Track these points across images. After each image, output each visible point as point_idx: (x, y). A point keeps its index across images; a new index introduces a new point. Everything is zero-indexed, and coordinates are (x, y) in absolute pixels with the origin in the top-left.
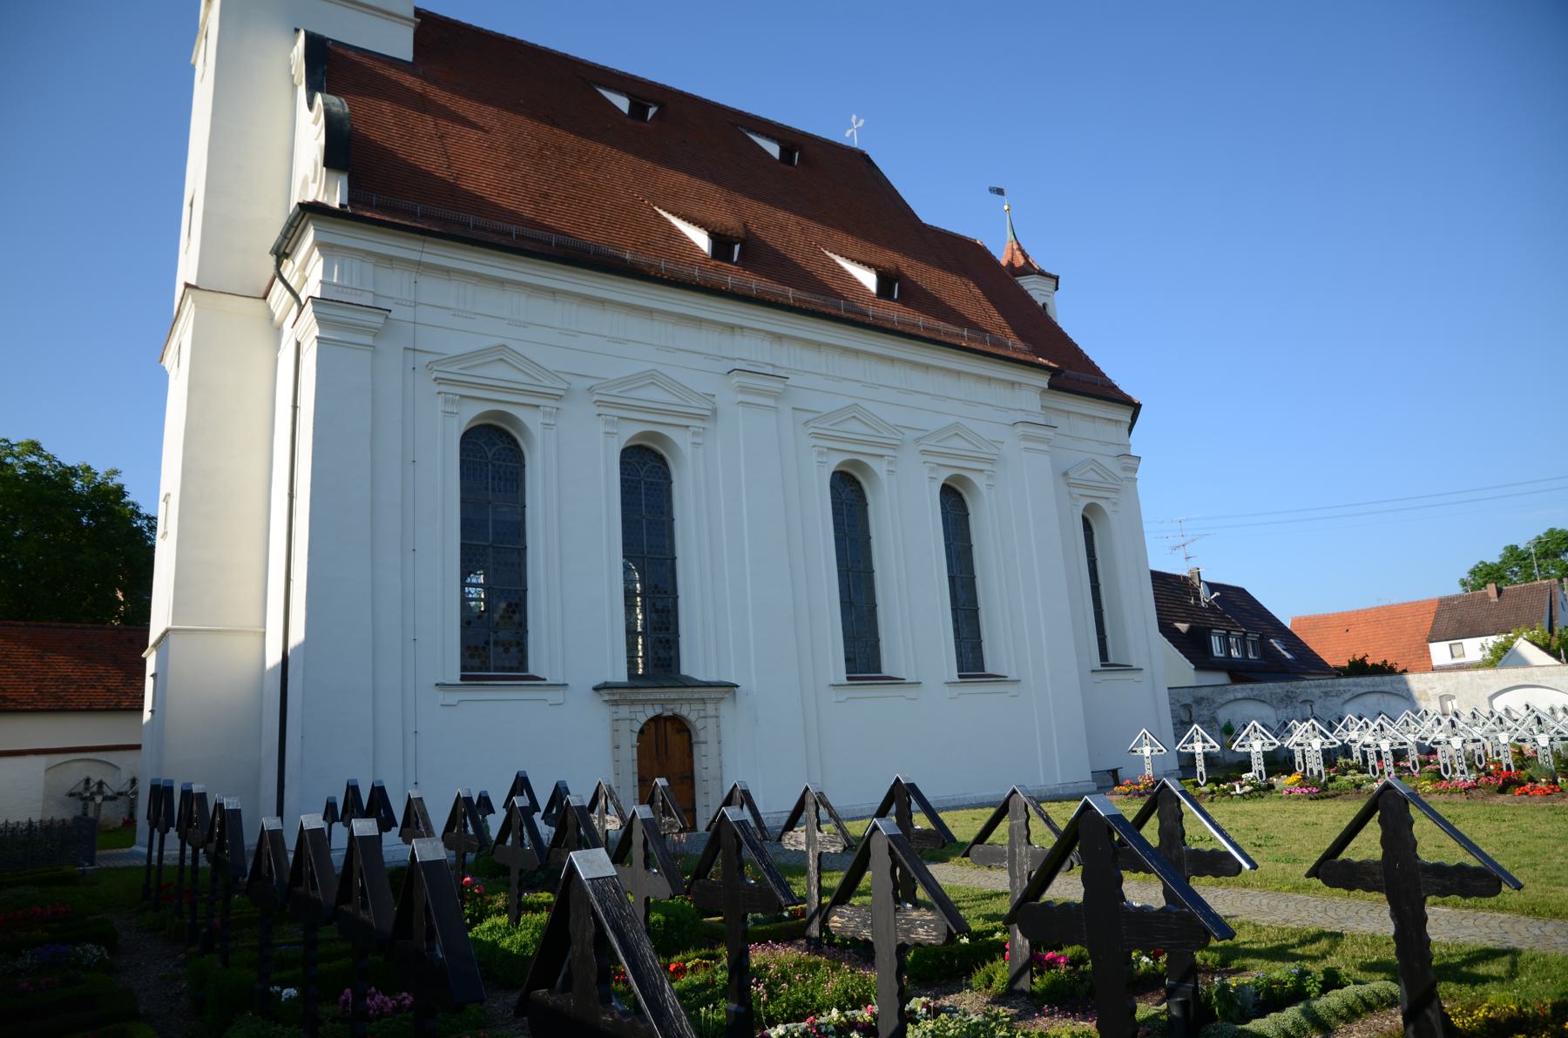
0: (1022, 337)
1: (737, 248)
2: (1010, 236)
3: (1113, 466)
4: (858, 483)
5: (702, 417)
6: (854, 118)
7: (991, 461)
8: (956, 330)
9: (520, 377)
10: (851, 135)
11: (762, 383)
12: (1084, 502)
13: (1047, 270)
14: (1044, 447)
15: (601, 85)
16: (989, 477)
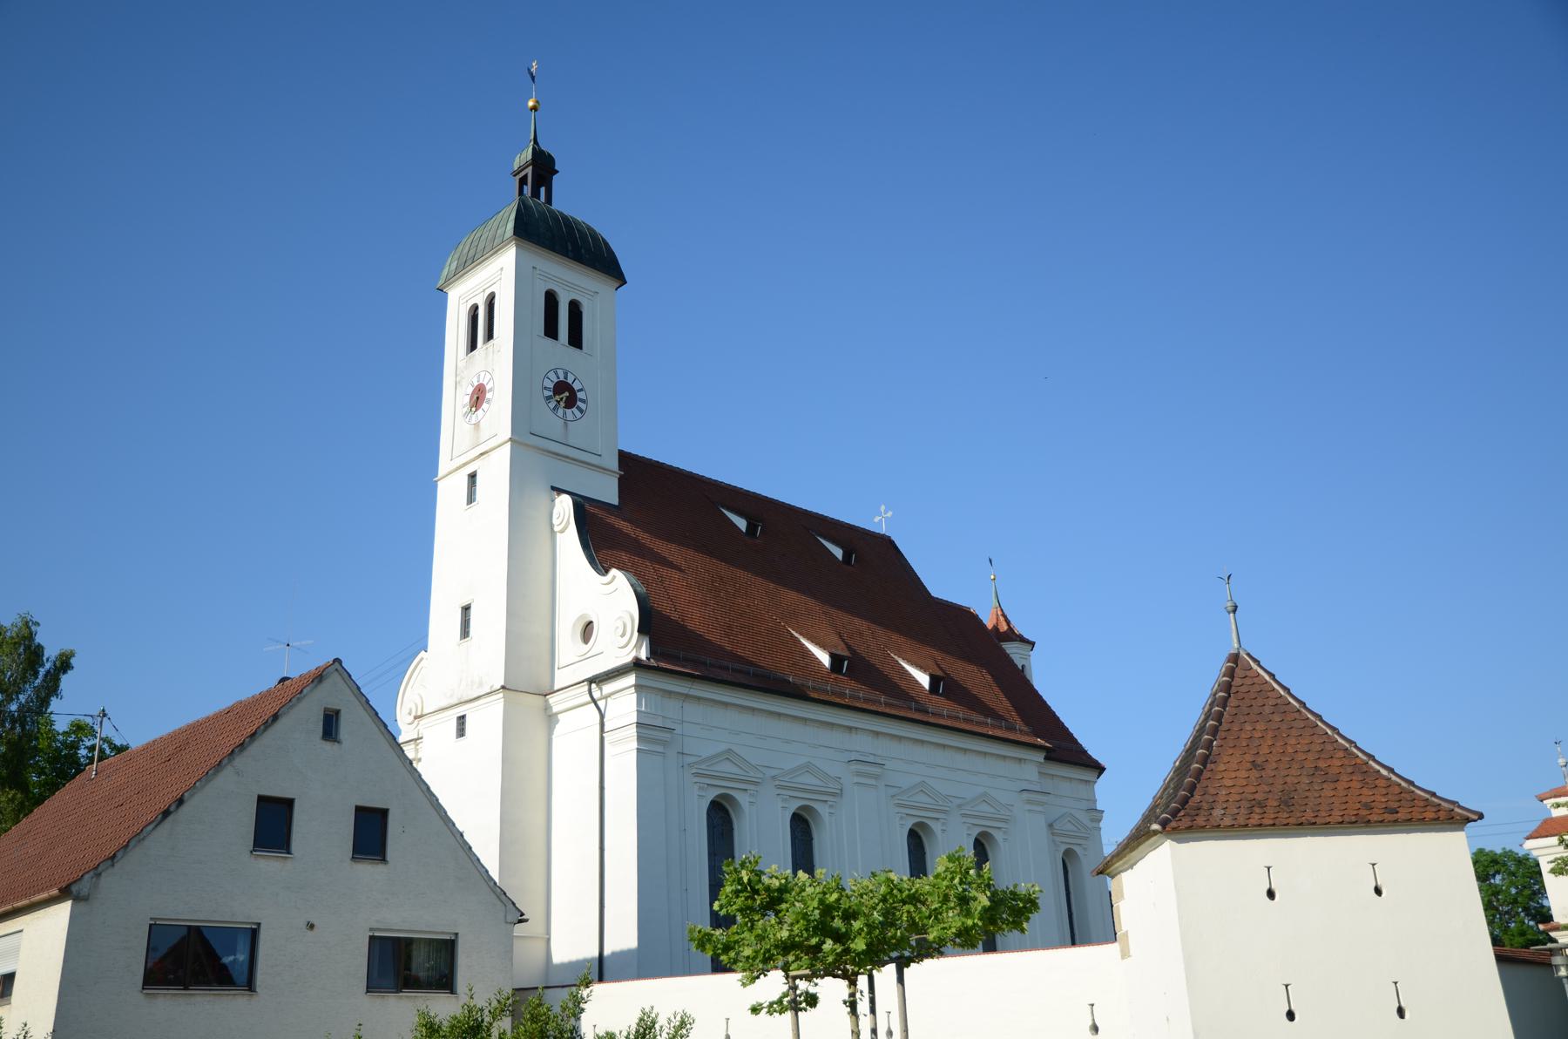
0: (1027, 724)
3: (1084, 818)
5: (834, 794)
6: (883, 508)
8: (981, 718)
10: (879, 522)
11: (869, 768)
12: (1063, 848)
13: (1026, 636)
14: (1039, 808)
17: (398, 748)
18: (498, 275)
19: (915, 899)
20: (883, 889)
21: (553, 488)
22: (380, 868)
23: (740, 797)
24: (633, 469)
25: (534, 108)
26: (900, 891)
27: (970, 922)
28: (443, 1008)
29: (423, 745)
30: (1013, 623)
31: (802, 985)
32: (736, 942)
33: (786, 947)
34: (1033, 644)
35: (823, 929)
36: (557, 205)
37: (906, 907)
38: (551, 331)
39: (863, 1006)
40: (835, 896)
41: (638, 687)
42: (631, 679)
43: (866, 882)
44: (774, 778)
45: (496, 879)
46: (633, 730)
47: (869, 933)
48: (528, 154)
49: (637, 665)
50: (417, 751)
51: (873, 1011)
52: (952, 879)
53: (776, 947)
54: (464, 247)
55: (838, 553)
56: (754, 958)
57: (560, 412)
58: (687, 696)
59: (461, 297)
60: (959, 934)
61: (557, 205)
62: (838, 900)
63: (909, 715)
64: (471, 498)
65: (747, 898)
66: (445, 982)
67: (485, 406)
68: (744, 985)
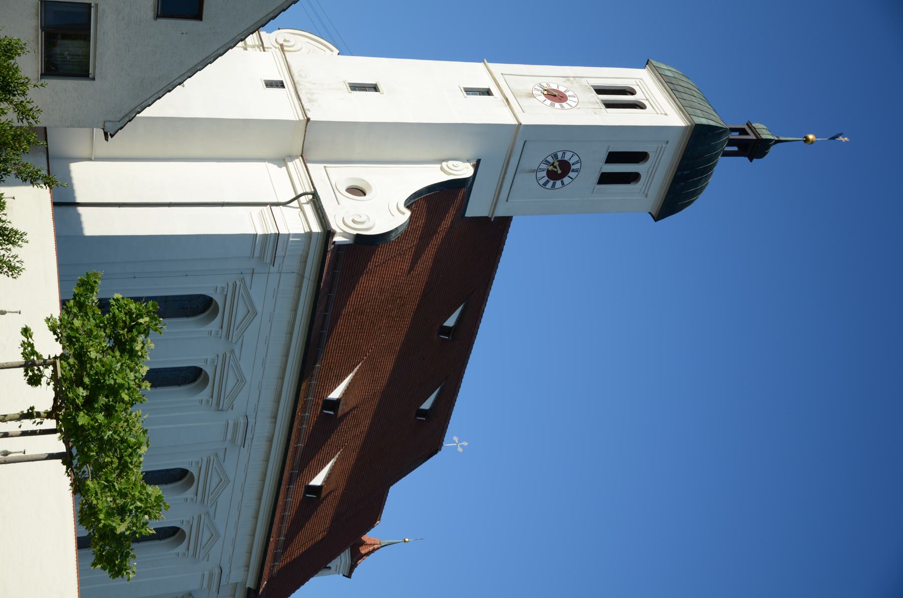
0: (279, 571)
1: (332, 413)
2: (386, 542)
4: (180, 479)
5: (218, 404)
6: (465, 444)
7: (194, 554)
8: (284, 531)
9: (239, 318)
10: (454, 440)
11: (241, 434)
14: (205, 586)
15: (465, 306)
16: (184, 554)
17: (256, 28)
18: (661, 111)
19: (123, 468)
20: (133, 440)
21: (479, 161)
22: (151, 13)
23: (214, 325)
24: (496, 230)
25: (807, 140)
26: (131, 455)
27: (102, 516)
28: (28, 64)
29: (258, 53)
30: (367, 559)
31: (48, 372)
32: (86, 314)
33: (81, 356)
34: (349, 576)
35: (97, 388)
36: (722, 161)
37: (116, 461)
38: (614, 157)
39: (28, 425)
40: (126, 398)
41: (309, 235)
42: (316, 228)
43: (138, 425)
44: (232, 351)
45: (144, 114)
46: (273, 231)
47: (93, 427)
48: (766, 135)
49: (328, 233)
50: (253, 47)
51: (25, 434)
52: (141, 500)
53: (82, 347)
54: (685, 82)
55: (427, 405)
56: (72, 329)
57: (544, 166)
58: (302, 276)
59: (642, 81)
60: (91, 507)
61: (722, 161)
62: (123, 400)
63: (287, 468)
64: (469, 91)
65: (124, 322)
66: (52, 68)
67: (548, 102)
68: (48, 320)
